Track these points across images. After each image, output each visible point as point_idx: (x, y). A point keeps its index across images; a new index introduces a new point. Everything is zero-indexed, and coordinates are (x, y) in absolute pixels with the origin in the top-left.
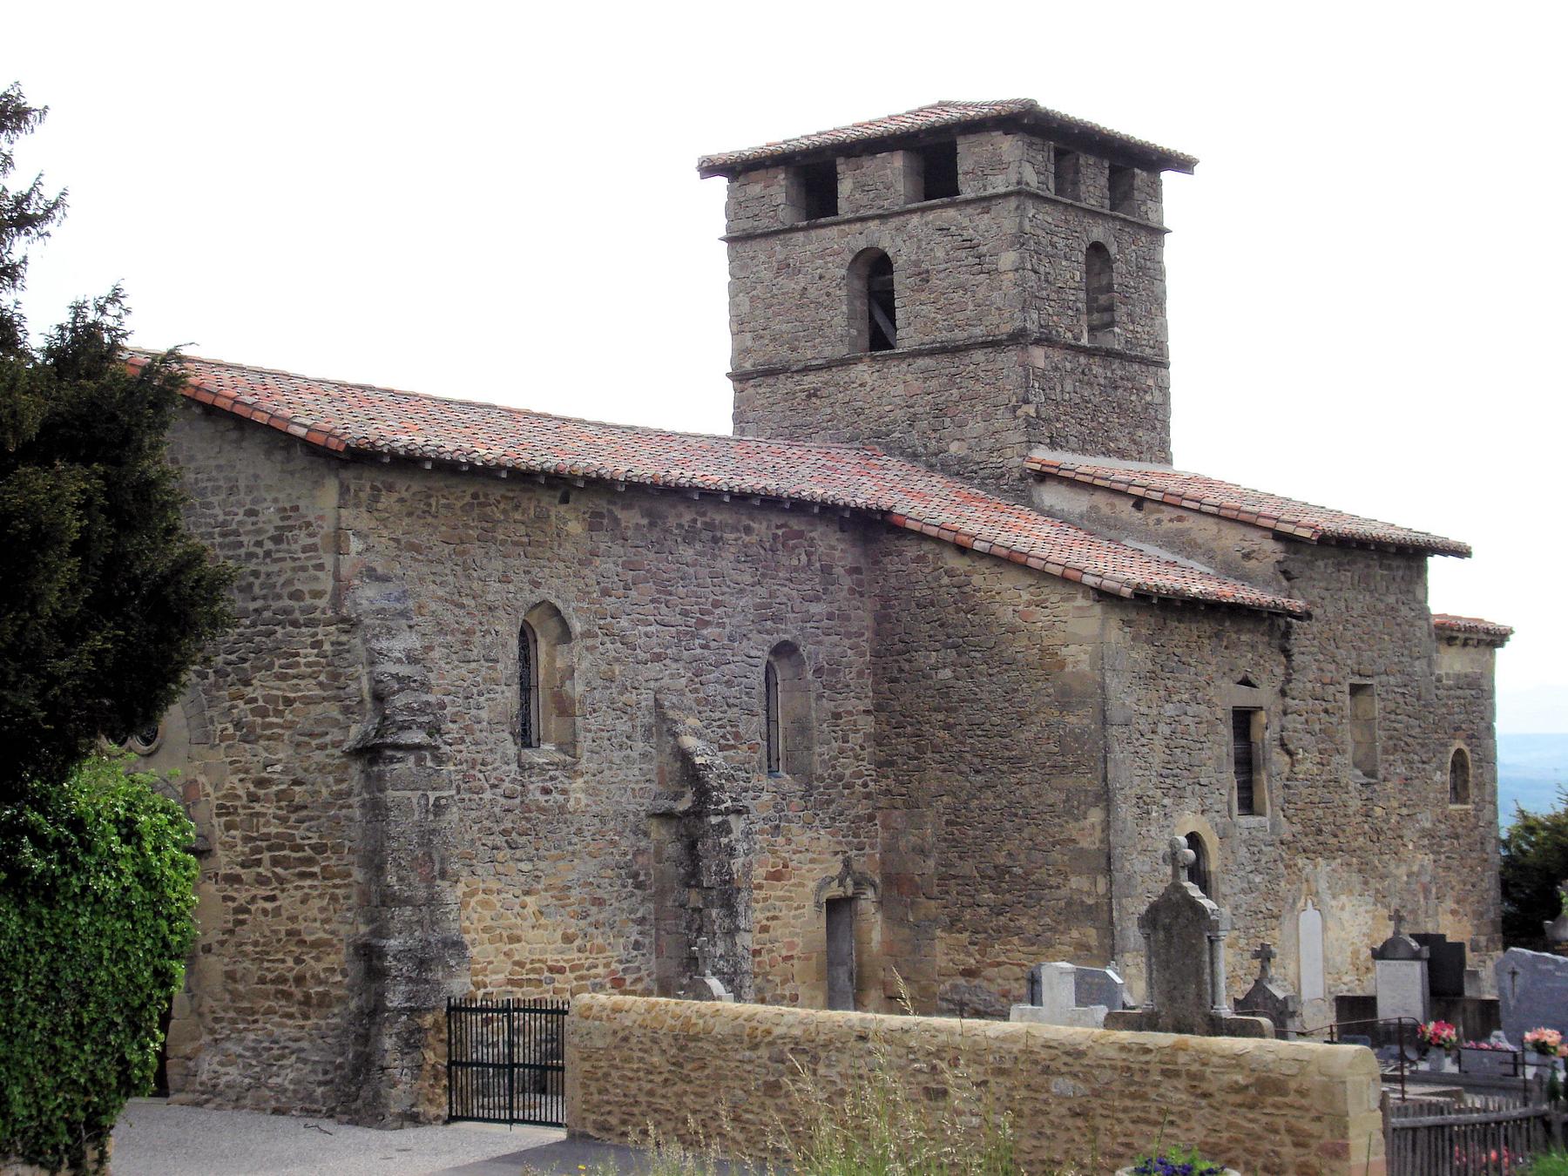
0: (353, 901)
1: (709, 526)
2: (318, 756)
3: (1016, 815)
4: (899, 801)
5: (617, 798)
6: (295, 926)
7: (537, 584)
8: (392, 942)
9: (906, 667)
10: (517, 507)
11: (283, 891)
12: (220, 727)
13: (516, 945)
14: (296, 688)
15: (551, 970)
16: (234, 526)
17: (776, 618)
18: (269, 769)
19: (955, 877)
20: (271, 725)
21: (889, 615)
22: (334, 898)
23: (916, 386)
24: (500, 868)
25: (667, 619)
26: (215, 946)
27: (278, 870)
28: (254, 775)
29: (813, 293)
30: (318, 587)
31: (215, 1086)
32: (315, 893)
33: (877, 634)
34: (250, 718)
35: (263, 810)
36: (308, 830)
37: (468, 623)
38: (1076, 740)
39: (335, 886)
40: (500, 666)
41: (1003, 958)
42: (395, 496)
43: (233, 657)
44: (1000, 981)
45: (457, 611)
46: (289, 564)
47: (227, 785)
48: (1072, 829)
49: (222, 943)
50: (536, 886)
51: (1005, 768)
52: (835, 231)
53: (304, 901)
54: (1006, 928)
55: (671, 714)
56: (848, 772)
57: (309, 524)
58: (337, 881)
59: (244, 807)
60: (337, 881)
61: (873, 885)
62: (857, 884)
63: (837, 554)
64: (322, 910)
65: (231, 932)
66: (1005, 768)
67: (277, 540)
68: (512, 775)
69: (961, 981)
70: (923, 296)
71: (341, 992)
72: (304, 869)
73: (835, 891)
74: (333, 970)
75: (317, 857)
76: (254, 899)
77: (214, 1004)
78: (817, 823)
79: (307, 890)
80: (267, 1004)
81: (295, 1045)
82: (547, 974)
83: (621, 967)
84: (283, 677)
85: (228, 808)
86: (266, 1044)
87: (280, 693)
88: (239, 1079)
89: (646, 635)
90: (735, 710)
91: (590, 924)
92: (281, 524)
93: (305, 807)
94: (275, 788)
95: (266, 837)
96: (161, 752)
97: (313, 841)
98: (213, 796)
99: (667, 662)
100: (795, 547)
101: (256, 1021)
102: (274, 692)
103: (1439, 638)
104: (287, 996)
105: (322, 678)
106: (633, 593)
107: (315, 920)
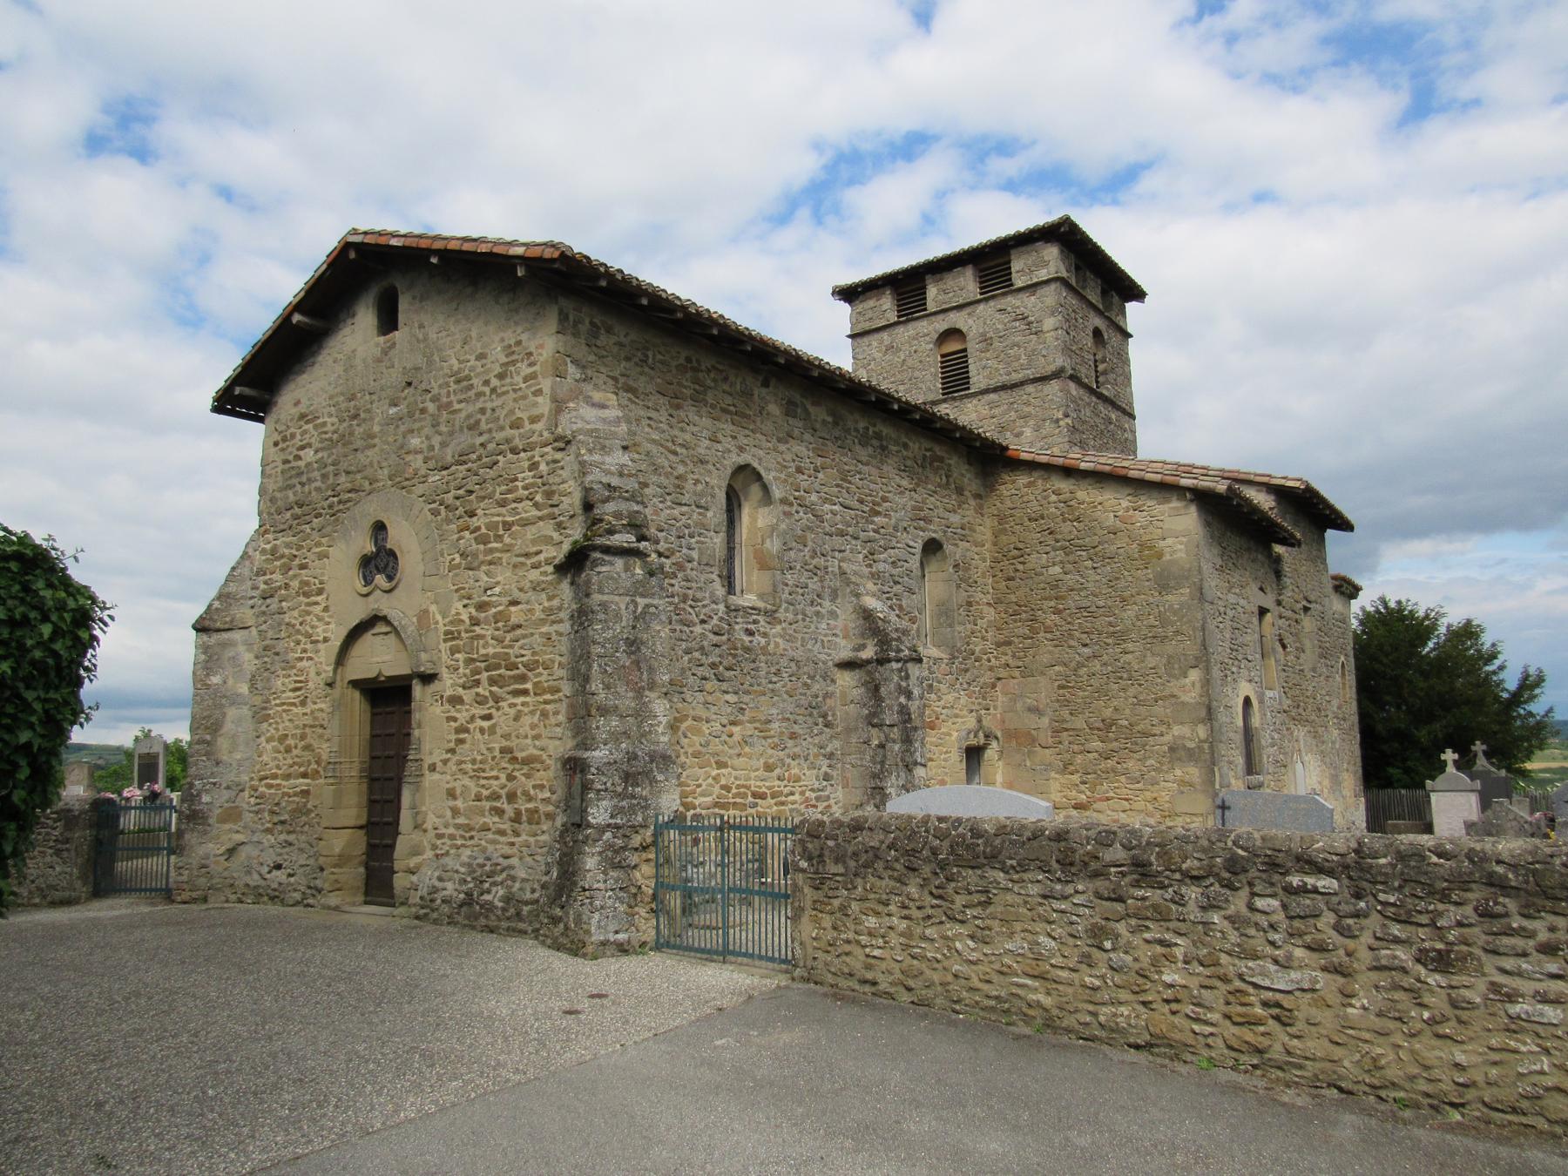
0: (561, 718)
1: (878, 436)
2: (534, 575)
3: (1121, 678)
4: (1016, 673)
5: (809, 647)
6: (508, 743)
7: (741, 449)
8: (596, 753)
9: (1020, 567)
10: (726, 379)
11: (498, 709)
12: (449, 558)
13: (723, 771)
14: (515, 511)
15: (754, 795)
16: (467, 372)
17: (927, 520)
18: (489, 593)
19: (1067, 730)
20: (492, 551)
21: (1005, 529)
22: (544, 714)
23: (985, 412)
24: (710, 699)
25: (847, 502)
26: (439, 764)
27: (494, 689)
28: (476, 599)
29: (910, 362)
30: (536, 412)
31: (432, 901)
32: (526, 710)
33: (995, 544)
34: (475, 546)
35: (483, 632)
36: (521, 648)
37: (681, 469)
38: (1175, 613)
39: (546, 702)
40: (710, 514)
41: (1111, 794)
42: (614, 339)
43: (461, 492)
44: (1109, 812)
45: (671, 457)
46: (512, 395)
47: (453, 612)
48: (1173, 687)
49: (445, 762)
50: (740, 717)
51: (1110, 641)
52: (924, 323)
53: (516, 719)
54: (1114, 770)
55: (853, 579)
56: (977, 649)
57: (531, 354)
58: (548, 697)
59: (467, 631)
60: (548, 697)
61: (997, 738)
62: (987, 736)
63: (966, 480)
64: (533, 726)
65: (452, 751)
66: (1110, 641)
67: (501, 376)
68: (720, 614)
69: (1074, 813)
70: (988, 355)
71: (551, 808)
72: (517, 686)
73: (973, 742)
74: (542, 787)
75: (530, 674)
76: (473, 718)
77: (437, 820)
78: (958, 686)
79: (519, 707)
80: (483, 820)
81: (505, 863)
82: (750, 799)
83: (813, 795)
84: (503, 503)
85: (452, 633)
86: (480, 861)
87: (500, 519)
88: (455, 894)
89: (832, 512)
90: (899, 586)
91: (789, 756)
92: (506, 360)
93: (519, 626)
94: (494, 610)
95: (485, 659)
96: (401, 586)
97: (524, 659)
98: (441, 625)
99: (848, 538)
100: (938, 468)
101: (472, 838)
102: (496, 519)
103: (1337, 589)
104: (500, 812)
105: (538, 498)
106: (820, 475)
107: (526, 737)
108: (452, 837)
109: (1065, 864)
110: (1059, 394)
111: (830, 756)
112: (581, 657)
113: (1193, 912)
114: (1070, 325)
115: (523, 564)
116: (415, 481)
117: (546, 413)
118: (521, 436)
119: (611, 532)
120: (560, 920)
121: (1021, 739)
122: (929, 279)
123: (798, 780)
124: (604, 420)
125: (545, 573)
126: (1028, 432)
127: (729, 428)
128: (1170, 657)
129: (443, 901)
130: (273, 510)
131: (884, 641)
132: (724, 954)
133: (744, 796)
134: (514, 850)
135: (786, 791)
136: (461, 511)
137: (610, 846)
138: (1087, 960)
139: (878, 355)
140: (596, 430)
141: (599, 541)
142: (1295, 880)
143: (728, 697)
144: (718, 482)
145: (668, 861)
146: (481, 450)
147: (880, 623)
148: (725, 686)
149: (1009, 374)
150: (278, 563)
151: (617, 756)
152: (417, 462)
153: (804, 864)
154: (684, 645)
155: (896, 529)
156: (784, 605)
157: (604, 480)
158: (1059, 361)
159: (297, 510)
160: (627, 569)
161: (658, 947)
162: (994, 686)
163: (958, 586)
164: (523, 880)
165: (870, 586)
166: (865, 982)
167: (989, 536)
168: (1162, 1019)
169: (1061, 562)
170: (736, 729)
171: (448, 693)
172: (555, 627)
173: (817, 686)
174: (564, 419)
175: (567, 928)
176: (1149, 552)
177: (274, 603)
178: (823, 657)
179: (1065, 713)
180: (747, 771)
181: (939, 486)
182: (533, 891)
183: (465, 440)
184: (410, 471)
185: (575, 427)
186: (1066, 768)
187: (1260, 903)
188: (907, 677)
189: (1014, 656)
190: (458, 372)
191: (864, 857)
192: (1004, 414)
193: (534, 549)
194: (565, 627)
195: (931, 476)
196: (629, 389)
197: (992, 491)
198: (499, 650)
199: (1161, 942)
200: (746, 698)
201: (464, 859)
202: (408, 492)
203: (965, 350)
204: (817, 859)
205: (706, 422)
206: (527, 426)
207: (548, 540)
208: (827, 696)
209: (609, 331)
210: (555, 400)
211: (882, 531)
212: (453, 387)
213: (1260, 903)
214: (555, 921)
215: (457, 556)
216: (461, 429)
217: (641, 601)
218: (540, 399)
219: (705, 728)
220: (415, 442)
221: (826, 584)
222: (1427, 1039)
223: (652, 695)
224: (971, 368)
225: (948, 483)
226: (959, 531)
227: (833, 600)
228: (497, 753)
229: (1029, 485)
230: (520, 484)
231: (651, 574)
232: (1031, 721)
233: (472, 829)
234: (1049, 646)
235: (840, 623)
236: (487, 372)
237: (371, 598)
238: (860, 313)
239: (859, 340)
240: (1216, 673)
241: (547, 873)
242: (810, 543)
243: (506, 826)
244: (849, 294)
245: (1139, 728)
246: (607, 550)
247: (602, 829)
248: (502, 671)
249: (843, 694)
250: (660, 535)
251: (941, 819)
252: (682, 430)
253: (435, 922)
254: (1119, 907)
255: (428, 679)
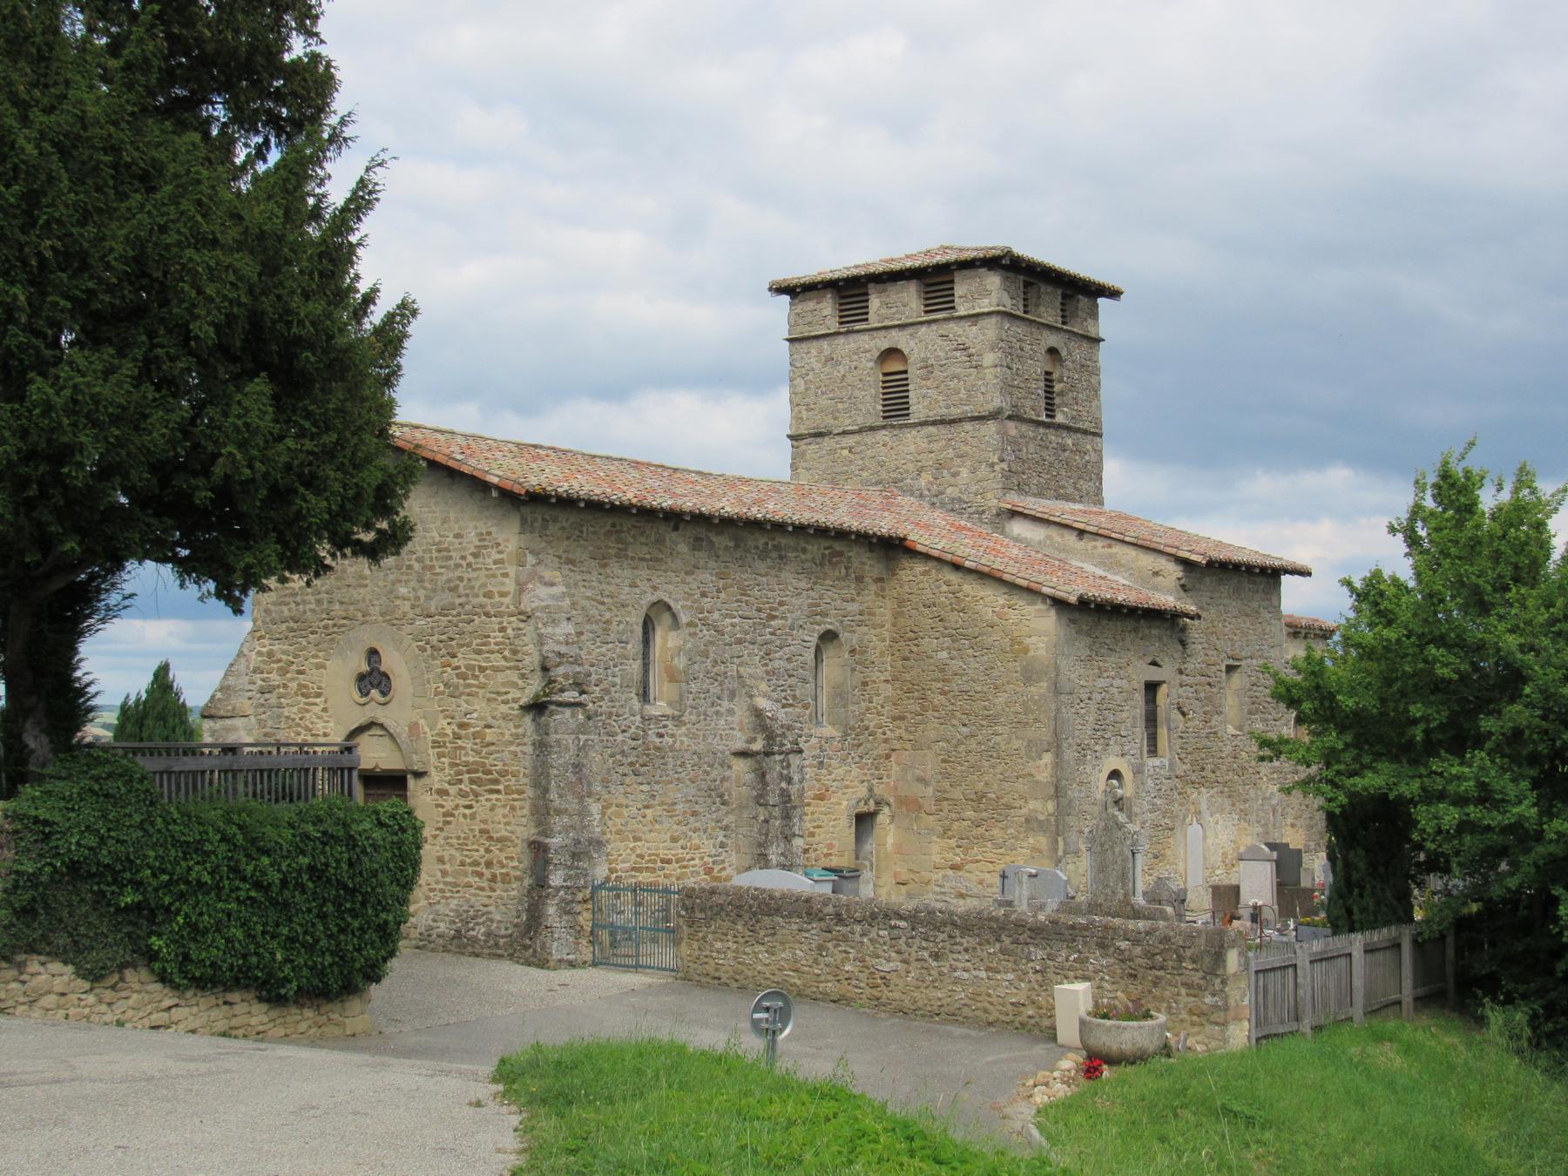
0: (525, 812)
2: (504, 708)
4: (908, 745)
7: (655, 588)
8: (554, 840)
9: (915, 649)
10: (642, 534)
15: (663, 861)
20: (470, 686)
22: (513, 808)
24: (629, 790)
27: (474, 787)
28: (458, 720)
29: (849, 379)
34: (455, 680)
37: (608, 615)
38: (1035, 703)
39: (514, 800)
43: (444, 637)
45: (601, 607)
46: (484, 572)
47: (439, 727)
48: (1031, 766)
50: (652, 802)
51: (984, 723)
53: (492, 809)
54: (982, 837)
56: (872, 724)
58: (515, 796)
60: (515, 796)
62: (878, 803)
63: (867, 568)
64: (505, 816)
65: (441, 829)
66: (984, 723)
67: (475, 555)
69: (950, 872)
70: (929, 383)
71: (518, 873)
73: (863, 809)
74: (512, 858)
76: (457, 807)
81: (485, 909)
84: (479, 652)
86: (465, 908)
95: (467, 764)
100: (837, 563)
104: (480, 875)
105: (506, 653)
106: (723, 595)
108: (442, 891)
109: (809, 914)
110: (996, 437)
111: (726, 828)
112: (542, 774)
113: (857, 938)
114: (1011, 353)
115: (495, 699)
116: (404, 622)
117: (512, 590)
118: (493, 606)
119: (562, 690)
120: (530, 947)
121: (910, 805)
122: (871, 286)
123: (698, 848)
124: (553, 596)
125: (513, 709)
126: (965, 473)
127: (644, 573)
128: (1030, 741)
129: (438, 936)
130: (268, 619)
131: (770, 737)
132: (637, 967)
133: (654, 862)
134: (491, 901)
135: (688, 857)
136: (443, 651)
137: (563, 900)
138: (816, 961)
139: (817, 366)
140: (547, 607)
141: (555, 698)
142: (893, 923)
143: (642, 787)
144: (636, 619)
145: (600, 910)
146: (460, 609)
147: (768, 721)
148: (640, 779)
149: (948, 407)
150: (275, 666)
151: (568, 841)
152: (406, 607)
153: (683, 913)
154: (609, 751)
155: (792, 628)
156: (689, 710)
157: (556, 649)
158: (996, 401)
159: (292, 624)
160: (573, 716)
161: (595, 964)
162: (888, 757)
163: (853, 670)
164: (499, 922)
165: (763, 686)
166: (715, 978)
167: (888, 617)
168: (845, 988)
169: (948, 648)
170: (648, 812)
171: (436, 786)
172: (520, 748)
173: (715, 772)
174: (525, 598)
175: (535, 951)
176: (1018, 648)
177: (273, 699)
178: (721, 748)
179: (946, 784)
180: (657, 842)
181: (838, 579)
182: (506, 929)
183: (448, 598)
184: (398, 614)
185: (533, 605)
186: (945, 833)
187: (881, 933)
188: (789, 766)
189: (906, 730)
190: (439, 543)
191: (715, 909)
192: (942, 450)
193: (503, 690)
194: (529, 749)
195: (830, 572)
196: (570, 562)
197: (894, 575)
198: (477, 759)
199: (845, 952)
200: (656, 787)
201: (452, 906)
202: (398, 629)
203: (905, 372)
204: (690, 909)
205: (627, 573)
206: (497, 599)
207: (515, 685)
208: (723, 779)
209: (555, 520)
210: (518, 583)
211: (779, 632)
212: (435, 554)
213: (881, 933)
214: (526, 947)
215: (441, 685)
216: (443, 589)
217: (583, 738)
218: (506, 580)
219: (625, 812)
220: (403, 590)
221: (725, 686)
222: (931, 988)
223: (590, 800)
224: (911, 394)
225: (847, 575)
226: (858, 617)
227: (731, 700)
228: (477, 833)
229: (925, 573)
230: (492, 641)
231: (589, 718)
232: (919, 790)
233: (458, 885)
234: (935, 723)
235: (736, 719)
236: (465, 549)
237: (367, 707)
238: (798, 314)
239: (797, 345)
240: (1070, 755)
241: (518, 917)
242: (712, 655)
243: (485, 884)
244: (795, 291)
245: (1003, 801)
246: (560, 704)
247: (558, 889)
248: (480, 775)
249: (738, 777)
250: (592, 669)
251: (756, 889)
252: (608, 583)
253: (433, 950)
254: (829, 935)
255: (419, 775)
